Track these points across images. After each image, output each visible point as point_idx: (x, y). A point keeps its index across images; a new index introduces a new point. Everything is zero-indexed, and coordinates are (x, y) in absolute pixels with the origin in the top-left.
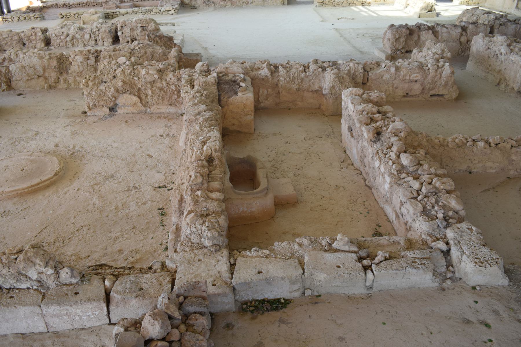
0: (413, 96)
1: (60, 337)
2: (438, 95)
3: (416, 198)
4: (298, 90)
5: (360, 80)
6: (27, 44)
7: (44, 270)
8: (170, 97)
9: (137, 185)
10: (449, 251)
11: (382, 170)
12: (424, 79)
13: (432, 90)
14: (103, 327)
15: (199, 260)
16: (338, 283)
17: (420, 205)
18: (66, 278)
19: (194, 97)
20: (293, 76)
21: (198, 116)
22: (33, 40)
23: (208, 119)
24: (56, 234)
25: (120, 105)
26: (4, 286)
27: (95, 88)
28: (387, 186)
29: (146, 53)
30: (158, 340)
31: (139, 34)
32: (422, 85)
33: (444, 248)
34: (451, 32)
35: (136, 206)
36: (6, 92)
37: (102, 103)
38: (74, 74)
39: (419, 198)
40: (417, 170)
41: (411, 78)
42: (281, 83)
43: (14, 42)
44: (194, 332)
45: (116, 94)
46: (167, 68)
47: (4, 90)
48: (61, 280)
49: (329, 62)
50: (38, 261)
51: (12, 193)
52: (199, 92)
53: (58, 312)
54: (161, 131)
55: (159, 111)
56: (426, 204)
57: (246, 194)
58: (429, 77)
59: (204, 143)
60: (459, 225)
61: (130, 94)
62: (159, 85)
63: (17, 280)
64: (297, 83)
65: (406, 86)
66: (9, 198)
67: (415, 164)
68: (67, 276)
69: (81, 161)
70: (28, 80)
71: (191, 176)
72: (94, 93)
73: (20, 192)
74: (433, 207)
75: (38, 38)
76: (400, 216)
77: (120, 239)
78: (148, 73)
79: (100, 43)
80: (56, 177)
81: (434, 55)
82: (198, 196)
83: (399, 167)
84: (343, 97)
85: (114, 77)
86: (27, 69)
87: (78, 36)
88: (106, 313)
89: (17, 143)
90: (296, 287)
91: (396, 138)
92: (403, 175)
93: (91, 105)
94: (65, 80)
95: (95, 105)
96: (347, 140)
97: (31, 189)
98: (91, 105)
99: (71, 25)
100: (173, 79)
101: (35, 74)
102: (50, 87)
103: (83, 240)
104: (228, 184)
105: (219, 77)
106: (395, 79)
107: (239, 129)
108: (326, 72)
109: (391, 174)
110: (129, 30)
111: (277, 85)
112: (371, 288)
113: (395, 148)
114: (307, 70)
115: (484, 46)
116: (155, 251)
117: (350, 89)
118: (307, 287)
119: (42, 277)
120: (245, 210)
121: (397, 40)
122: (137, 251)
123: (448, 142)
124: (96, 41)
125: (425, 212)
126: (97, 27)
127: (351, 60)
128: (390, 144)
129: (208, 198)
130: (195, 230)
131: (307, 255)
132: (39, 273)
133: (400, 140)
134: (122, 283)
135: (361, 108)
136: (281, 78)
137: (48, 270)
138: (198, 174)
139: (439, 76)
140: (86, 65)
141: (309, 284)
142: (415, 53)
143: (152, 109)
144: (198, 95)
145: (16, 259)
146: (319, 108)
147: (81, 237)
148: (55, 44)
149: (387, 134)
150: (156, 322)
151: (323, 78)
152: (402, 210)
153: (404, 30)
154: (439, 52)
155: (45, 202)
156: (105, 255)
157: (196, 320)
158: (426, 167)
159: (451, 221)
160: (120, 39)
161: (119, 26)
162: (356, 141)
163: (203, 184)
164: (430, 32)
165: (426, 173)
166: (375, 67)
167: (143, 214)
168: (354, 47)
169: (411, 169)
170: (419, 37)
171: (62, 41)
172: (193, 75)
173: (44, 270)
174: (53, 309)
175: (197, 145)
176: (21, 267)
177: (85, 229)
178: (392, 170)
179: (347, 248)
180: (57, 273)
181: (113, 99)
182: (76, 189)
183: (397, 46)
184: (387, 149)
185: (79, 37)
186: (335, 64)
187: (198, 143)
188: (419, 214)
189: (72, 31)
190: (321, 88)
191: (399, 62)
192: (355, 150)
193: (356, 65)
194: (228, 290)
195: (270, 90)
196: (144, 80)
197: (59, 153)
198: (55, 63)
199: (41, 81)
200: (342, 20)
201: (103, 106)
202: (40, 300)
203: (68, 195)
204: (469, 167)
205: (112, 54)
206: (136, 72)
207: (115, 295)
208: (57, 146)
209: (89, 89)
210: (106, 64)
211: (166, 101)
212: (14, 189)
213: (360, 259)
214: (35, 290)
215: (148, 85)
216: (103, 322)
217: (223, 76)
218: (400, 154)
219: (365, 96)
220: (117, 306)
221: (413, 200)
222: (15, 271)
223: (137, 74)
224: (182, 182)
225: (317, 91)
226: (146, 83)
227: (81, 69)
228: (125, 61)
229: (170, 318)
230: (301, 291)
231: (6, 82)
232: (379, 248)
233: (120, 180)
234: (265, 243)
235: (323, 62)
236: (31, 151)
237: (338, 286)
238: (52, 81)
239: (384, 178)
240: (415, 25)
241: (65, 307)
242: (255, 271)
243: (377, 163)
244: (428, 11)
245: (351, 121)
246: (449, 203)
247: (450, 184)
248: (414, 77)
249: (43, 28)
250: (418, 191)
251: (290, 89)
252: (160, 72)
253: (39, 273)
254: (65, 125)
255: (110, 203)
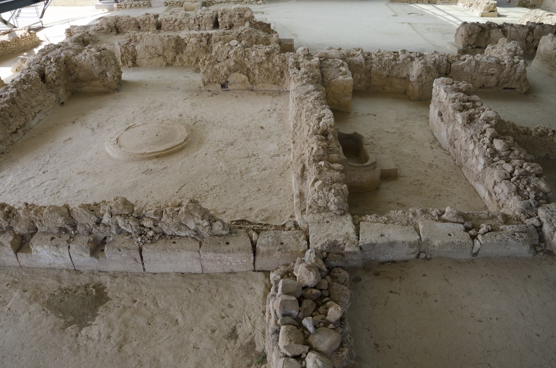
0: (488, 88)
1: (213, 278)
2: (511, 88)
3: (509, 179)
4: (388, 76)
5: (443, 70)
6: (142, 28)
7: (201, 222)
8: (275, 77)
9: (255, 153)
10: (541, 226)
11: (477, 152)
12: (500, 73)
13: (506, 83)
14: (249, 272)
15: (328, 222)
16: (449, 249)
17: (514, 186)
18: (218, 230)
19: (302, 78)
20: (385, 64)
21: (308, 95)
22: (147, 24)
23: (318, 98)
24: (194, 191)
25: (231, 82)
26: (167, 232)
27: (211, 66)
28: (480, 167)
29: (251, 37)
30: (311, 288)
31: (237, 21)
32: (497, 78)
33: (538, 224)
34: (519, 32)
35: (258, 171)
36: (131, 69)
37: (215, 80)
38: (188, 54)
39: (512, 180)
40: (509, 154)
41: (489, 71)
42: (373, 69)
43: (132, 26)
44: (339, 282)
45: (228, 72)
46: (273, 51)
47: (129, 67)
48: (214, 231)
49: (417, 53)
50: (196, 214)
51: (152, 155)
52: (306, 73)
53: (213, 258)
54: (268, 106)
55: (264, 89)
56: (519, 185)
57: (357, 167)
58: (505, 71)
59: (319, 119)
60: (548, 205)
61: (240, 73)
62: (266, 66)
63: (179, 229)
64: (387, 70)
65: (483, 78)
66: (150, 159)
67: (507, 149)
68: (220, 228)
69: (204, 129)
70: (150, 58)
71: (313, 148)
72: (209, 71)
73: (159, 154)
74: (525, 188)
75: (151, 22)
76: (493, 194)
77: (248, 199)
78: (257, 55)
79: (203, 26)
80: (186, 142)
81: (508, 52)
82: (321, 166)
83: (493, 151)
84: (434, 85)
85: (228, 58)
86: (150, 48)
87: (184, 21)
88: (252, 262)
89: (147, 112)
90: (413, 250)
91: (488, 125)
92: (496, 158)
93: (206, 81)
94: (181, 59)
95: (209, 81)
96: (435, 123)
97: (167, 152)
98: (206, 81)
99: (179, 12)
100: (278, 61)
101: (156, 54)
102: (168, 65)
103: (217, 198)
104: (343, 157)
105: (320, 61)
106: (474, 72)
107: (337, 109)
108: (414, 62)
109: (485, 156)
110: (228, 16)
111: (370, 71)
112: (476, 254)
113: (488, 134)
114: (397, 59)
115: (552, 46)
116: (281, 211)
117: (442, 78)
118: (422, 250)
119: (198, 228)
120: (357, 180)
121: (470, 36)
122: (265, 210)
123: (531, 132)
124: (199, 25)
125: (518, 192)
126: (201, 14)
127: (435, 52)
128: (483, 130)
129: (330, 168)
130: (322, 195)
131: (421, 224)
132: (196, 224)
133: (491, 127)
134: (264, 237)
135: (453, 95)
136: (374, 65)
137: (204, 222)
138: (320, 147)
139: (513, 71)
140: (199, 46)
141: (424, 248)
142: (489, 49)
143: (258, 87)
144: (305, 76)
145: (178, 211)
146: (405, 93)
147: (215, 195)
148: (165, 28)
149: (480, 121)
150: (311, 273)
151: (411, 66)
152: (495, 189)
153: (477, 27)
154: (513, 49)
155: (180, 164)
156: (237, 212)
157: (340, 273)
158: (516, 152)
159: (541, 201)
160: (220, 24)
161: (219, 13)
162: (446, 125)
163: (324, 156)
164: (500, 30)
165: (517, 158)
166: (457, 60)
167: (265, 179)
168: (427, 40)
169: (503, 154)
170: (489, 34)
171: (171, 26)
172: (298, 58)
173: (201, 222)
174: (210, 255)
175: (314, 121)
176: (183, 218)
177: (218, 188)
178: (486, 153)
179: (455, 220)
180: (211, 225)
181: (225, 77)
182: (204, 154)
183: (469, 42)
184: (481, 134)
185: (185, 22)
186: (421, 55)
187: (314, 119)
188: (513, 194)
189: (179, 17)
190: (408, 76)
191: (478, 57)
192: (445, 133)
193: (441, 57)
194: (357, 249)
195: (363, 75)
196: (253, 61)
197: (183, 122)
198: (173, 44)
199: (161, 59)
200: (413, 15)
201: (216, 82)
202: (198, 247)
203: (197, 158)
204: (547, 154)
205: (222, 37)
206: (247, 54)
207: (260, 247)
208: (180, 115)
209: (205, 67)
210: (220, 46)
211: (270, 80)
212: (154, 151)
213: (467, 229)
214: (193, 238)
215: (256, 66)
216: (249, 269)
217: (324, 60)
218: (493, 140)
219: (454, 85)
220: (263, 256)
221: (507, 181)
222: (178, 221)
223: (248, 56)
224: (303, 152)
225: (405, 78)
226: (255, 63)
227: (195, 50)
228: (236, 44)
229: (320, 270)
230: (417, 253)
231: (132, 60)
232: (480, 221)
233: (240, 148)
234: (379, 210)
235: (411, 53)
236: (160, 119)
237: (448, 252)
238: (169, 59)
239: (477, 160)
240: (487, 23)
241: (219, 254)
242: (378, 235)
243: (471, 147)
244: (491, 11)
245: (442, 107)
246: (539, 185)
247: (538, 168)
248: (491, 71)
249: (155, 14)
250: (511, 173)
251: (381, 75)
252: (268, 54)
253: (196, 224)
254: (185, 98)
255: (235, 167)
